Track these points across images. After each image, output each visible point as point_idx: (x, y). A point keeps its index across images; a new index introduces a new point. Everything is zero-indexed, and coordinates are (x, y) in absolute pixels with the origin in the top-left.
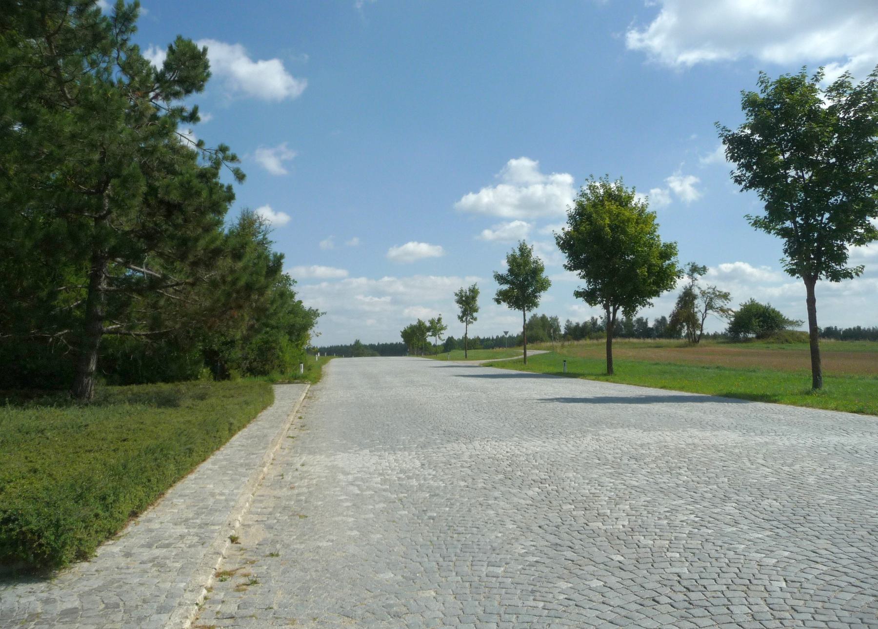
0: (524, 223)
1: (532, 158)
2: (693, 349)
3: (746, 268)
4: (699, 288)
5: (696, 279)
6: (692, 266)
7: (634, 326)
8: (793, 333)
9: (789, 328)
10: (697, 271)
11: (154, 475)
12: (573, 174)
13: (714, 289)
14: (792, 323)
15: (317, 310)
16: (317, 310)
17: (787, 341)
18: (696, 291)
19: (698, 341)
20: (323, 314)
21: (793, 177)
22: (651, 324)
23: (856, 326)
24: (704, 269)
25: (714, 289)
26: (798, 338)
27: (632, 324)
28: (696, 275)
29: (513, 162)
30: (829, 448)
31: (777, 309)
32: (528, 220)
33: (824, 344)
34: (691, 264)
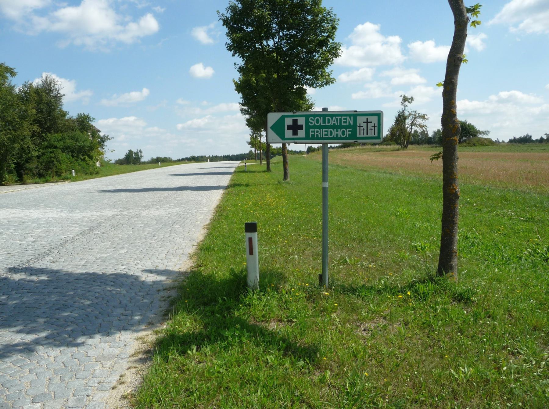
0: (367, 70)
1: (374, 23)
2: (405, 152)
3: (518, 94)
4: (408, 112)
5: (407, 106)
6: (404, 97)
7: (419, 136)
8: (480, 139)
9: (480, 136)
10: (407, 100)
11: (434, 216)
12: (400, 36)
13: (415, 112)
14: (482, 133)
15: (108, 136)
16: (108, 136)
17: (474, 145)
18: (407, 114)
19: (407, 147)
20: (112, 138)
21: (282, 32)
22: (430, 134)
23: (525, 135)
24: (412, 99)
25: (415, 112)
26: (482, 142)
27: (418, 135)
28: (407, 103)
29: (360, 27)
30: (39, 248)
31: (472, 124)
32: (370, 67)
33: (289, 156)
34: (403, 96)
